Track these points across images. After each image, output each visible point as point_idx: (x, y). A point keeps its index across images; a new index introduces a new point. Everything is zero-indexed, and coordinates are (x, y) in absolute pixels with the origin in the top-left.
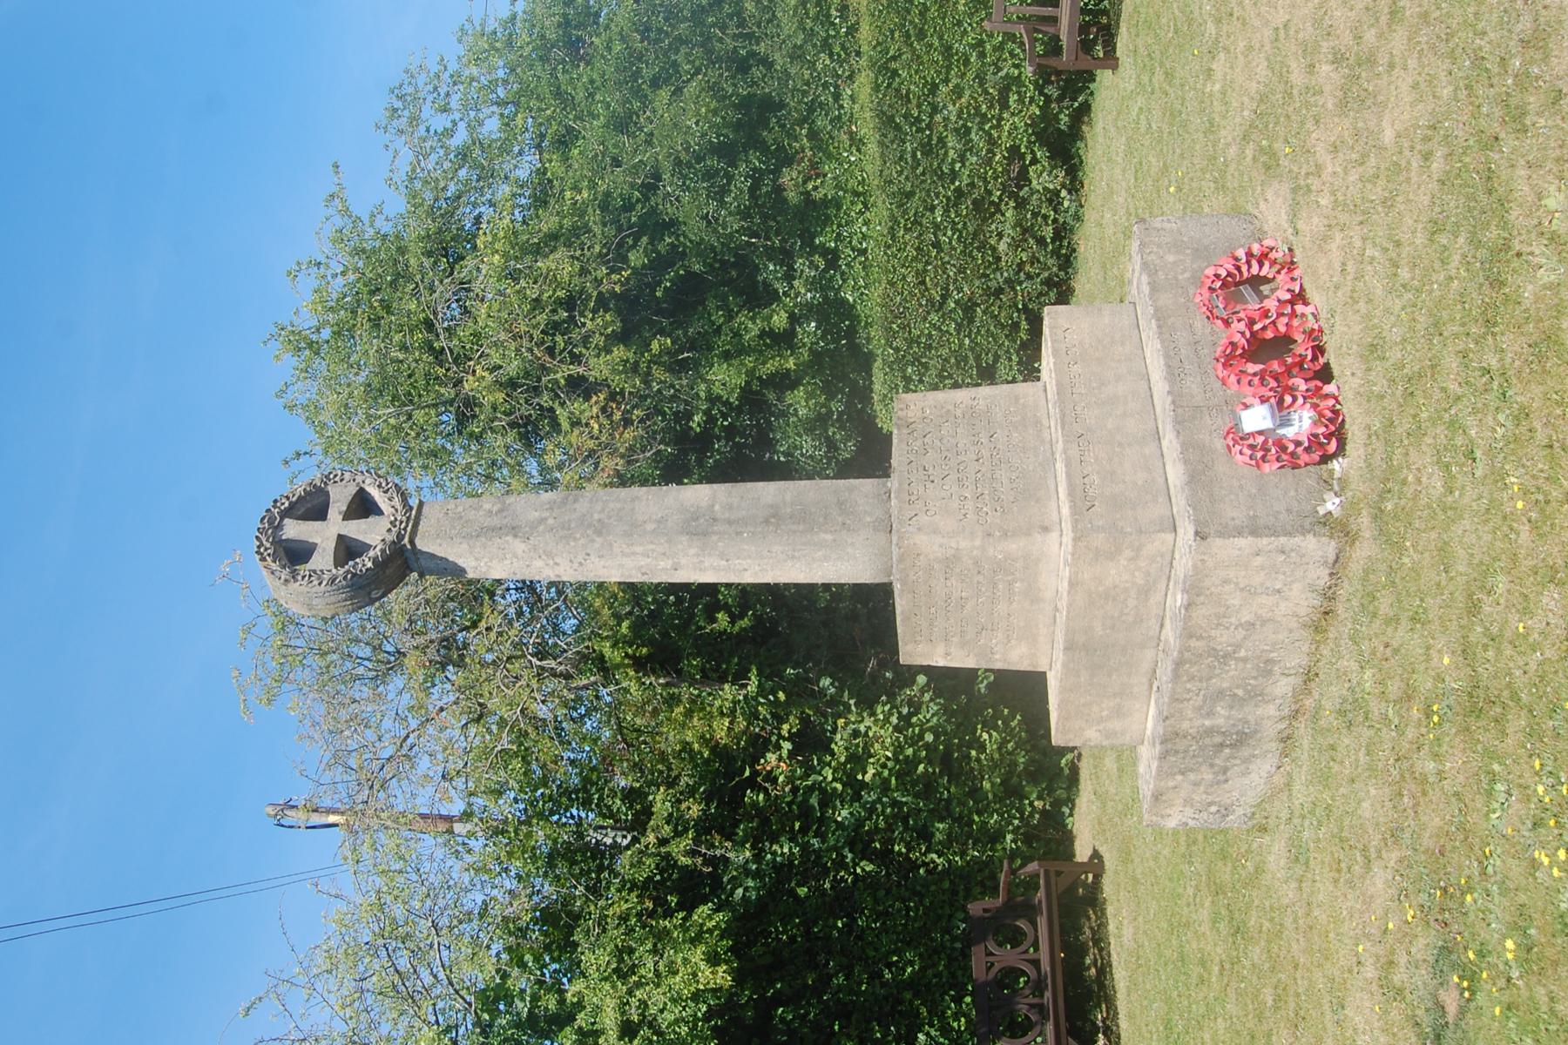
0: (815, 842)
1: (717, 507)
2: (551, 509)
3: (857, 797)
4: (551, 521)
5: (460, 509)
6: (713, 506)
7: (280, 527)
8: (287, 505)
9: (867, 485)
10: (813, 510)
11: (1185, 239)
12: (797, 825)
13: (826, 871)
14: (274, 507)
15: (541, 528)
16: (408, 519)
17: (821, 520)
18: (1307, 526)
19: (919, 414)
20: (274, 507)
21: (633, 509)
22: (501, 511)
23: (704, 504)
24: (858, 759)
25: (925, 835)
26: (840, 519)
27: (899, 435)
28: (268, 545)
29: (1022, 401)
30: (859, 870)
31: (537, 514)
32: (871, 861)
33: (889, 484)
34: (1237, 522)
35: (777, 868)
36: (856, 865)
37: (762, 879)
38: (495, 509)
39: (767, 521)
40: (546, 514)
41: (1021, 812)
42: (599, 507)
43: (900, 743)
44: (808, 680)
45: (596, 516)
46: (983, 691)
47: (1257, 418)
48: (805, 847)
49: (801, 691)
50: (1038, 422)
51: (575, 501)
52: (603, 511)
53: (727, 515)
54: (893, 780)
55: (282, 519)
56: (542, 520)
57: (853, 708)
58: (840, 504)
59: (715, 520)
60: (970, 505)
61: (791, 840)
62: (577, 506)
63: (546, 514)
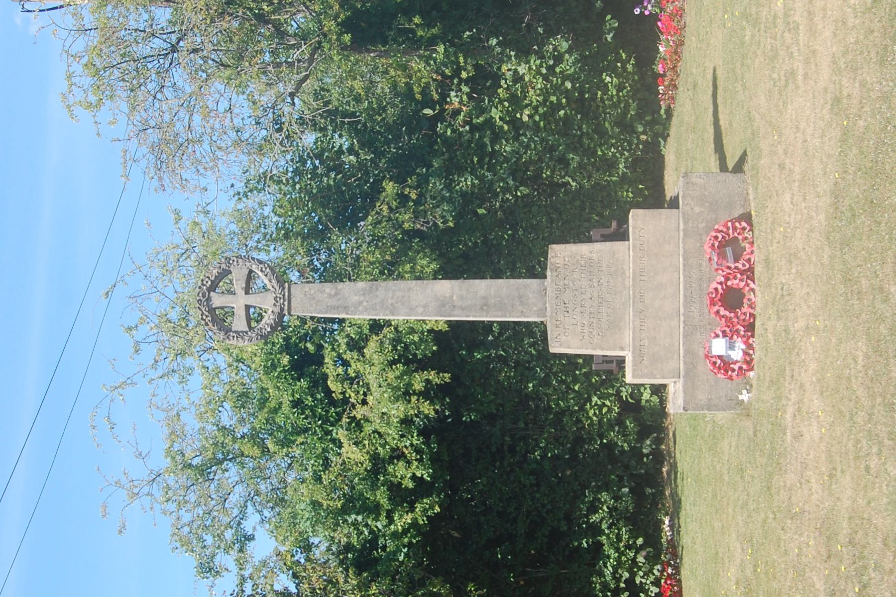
0: (489, 175)
1: (455, 298)
2: (364, 294)
3: (516, 138)
4: (365, 304)
5: (312, 292)
6: (453, 296)
7: (209, 299)
8: (210, 283)
9: (534, 283)
10: (506, 301)
11: (707, 194)
12: (476, 159)
13: (496, 195)
14: (203, 285)
15: (360, 308)
16: (284, 295)
17: (510, 309)
18: (733, 406)
19: (562, 262)
20: (203, 285)
21: (409, 297)
22: (336, 294)
23: (447, 295)
24: (516, 101)
25: (563, 161)
26: (520, 308)
27: (552, 276)
28: (207, 314)
29: (616, 256)
30: (519, 194)
31: (357, 298)
32: (526, 186)
33: (546, 283)
34: (703, 402)
35: (463, 194)
36: (517, 189)
37: (453, 203)
38: (333, 293)
39: (482, 309)
40: (362, 298)
41: (630, 144)
42: (390, 295)
43: (547, 89)
44: (481, 40)
45: (390, 301)
46: (609, 39)
47: (719, 347)
48: (481, 178)
49: (475, 48)
50: (623, 273)
51: (377, 289)
52: (393, 298)
53: (460, 304)
54: (542, 123)
55: (209, 293)
56: (360, 303)
57: (513, 58)
58: (520, 297)
59: (454, 306)
60: (586, 329)
61: (471, 174)
62: (378, 293)
63: (362, 298)
